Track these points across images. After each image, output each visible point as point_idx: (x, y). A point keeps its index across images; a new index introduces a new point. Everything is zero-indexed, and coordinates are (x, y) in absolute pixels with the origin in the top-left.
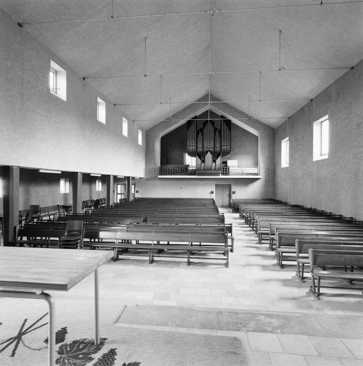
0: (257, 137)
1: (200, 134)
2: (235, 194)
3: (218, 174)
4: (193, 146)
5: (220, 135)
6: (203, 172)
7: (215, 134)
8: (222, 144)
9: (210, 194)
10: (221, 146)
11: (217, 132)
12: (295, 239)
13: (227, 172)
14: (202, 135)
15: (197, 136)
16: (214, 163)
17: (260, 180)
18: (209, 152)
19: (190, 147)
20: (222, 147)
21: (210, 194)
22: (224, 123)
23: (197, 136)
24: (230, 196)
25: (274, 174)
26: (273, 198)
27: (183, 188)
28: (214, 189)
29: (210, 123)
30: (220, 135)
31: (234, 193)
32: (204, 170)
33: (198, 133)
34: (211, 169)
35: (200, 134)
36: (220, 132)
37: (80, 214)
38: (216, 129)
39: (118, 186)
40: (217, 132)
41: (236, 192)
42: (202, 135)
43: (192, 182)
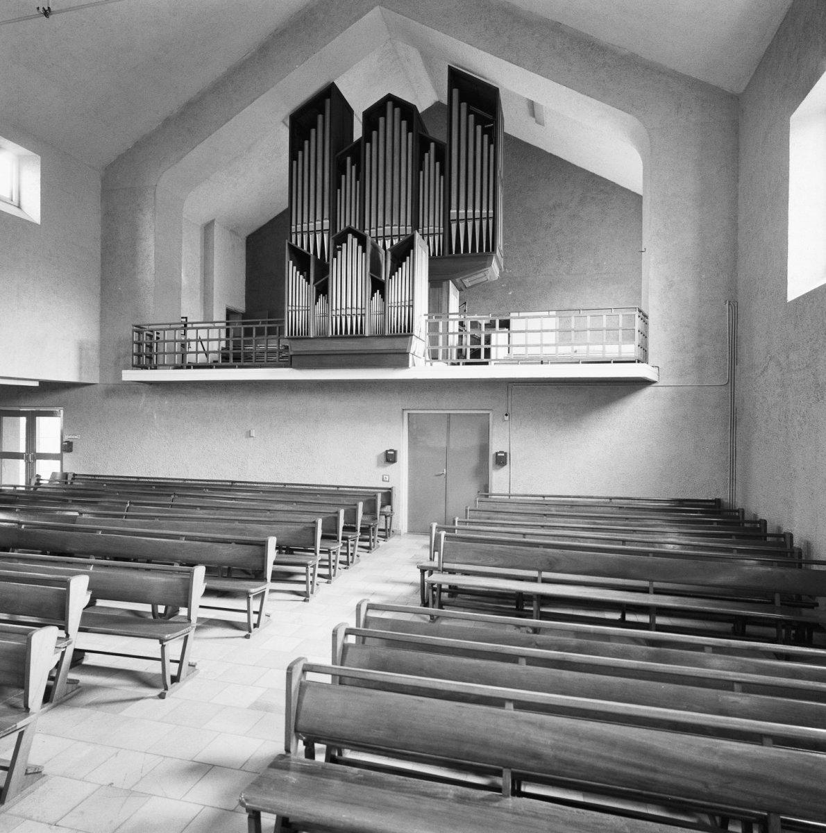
0: (638, 198)
1: (351, 170)
2: (506, 468)
3: (400, 357)
4: (315, 232)
5: (445, 171)
6: (322, 346)
7: (419, 165)
8: (453, 211)
9: (378, 465)
10: (447, 222)
11: (430, 157)
12: (775, 593)
13: (483, 346)
14: (360, 175)
15: (336, 184)
16: (377, 294)
17: (649, 390)
18: (350, 236)
19: (305, 237)
20: (454, 226)
21: (378, 465)
22: (472, 117)
23: (336, 184)
24: (482, 473)
25: (734, 359)
26: (724, 496)
27: (253, 434)
28: (400, 442)
29: (397, 110)
30: (445, 171)
31: (501, 460)
32: (322, 336)
33: (339, 170)
34: (360, 335)
35: (351, 170)
36: (442, 155)
37: (176, 481)
38: (422, 144)
39: (41, 422)
40: (430, 157)
41: (514, 458)
42: (360, 175)
43: (296, 403)
